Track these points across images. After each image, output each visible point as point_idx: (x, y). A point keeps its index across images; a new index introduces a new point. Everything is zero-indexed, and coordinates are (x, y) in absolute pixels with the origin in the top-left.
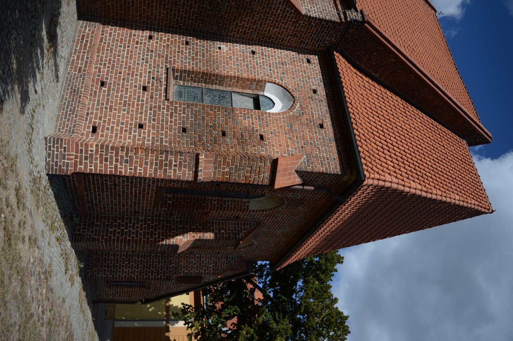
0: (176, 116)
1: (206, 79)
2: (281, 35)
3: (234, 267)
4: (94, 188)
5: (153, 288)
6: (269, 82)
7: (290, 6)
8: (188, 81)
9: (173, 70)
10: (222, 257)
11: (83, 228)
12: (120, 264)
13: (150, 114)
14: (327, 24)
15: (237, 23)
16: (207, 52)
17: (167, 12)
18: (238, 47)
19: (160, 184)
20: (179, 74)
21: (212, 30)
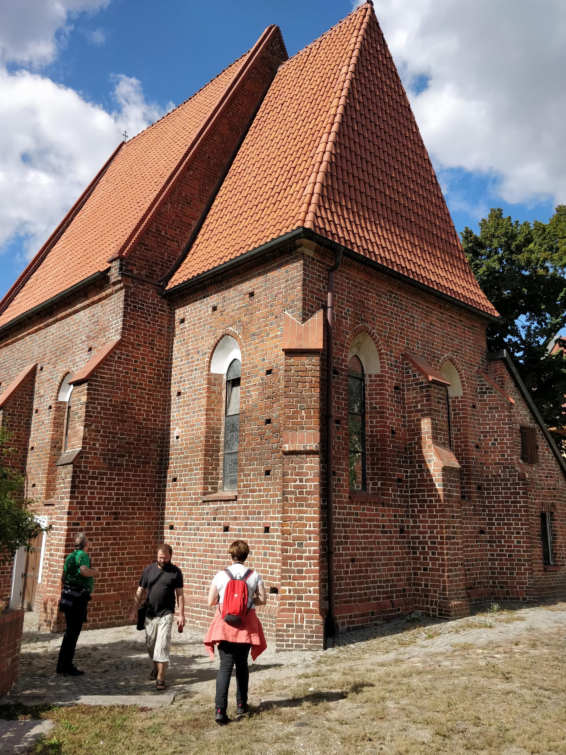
0: (254, 485)
1: (213, 451)
2: (154, 361)
3: (499, 381)
4: (361, 589)
5: (551, 500)
6: (209, 370)
7: (111, 357)
8: (218, 474)
9: (204, 494)
10: (480, 401)
11: (431, 605)
12: (507, 551)
13: (253, 519)
14: (130, 305)
15: (144, 420)
16: (183, 453)
17: (138, 509)
18: (174, 414)
19: (345, 498)
20: (209, 487)
21: (157, 450)
